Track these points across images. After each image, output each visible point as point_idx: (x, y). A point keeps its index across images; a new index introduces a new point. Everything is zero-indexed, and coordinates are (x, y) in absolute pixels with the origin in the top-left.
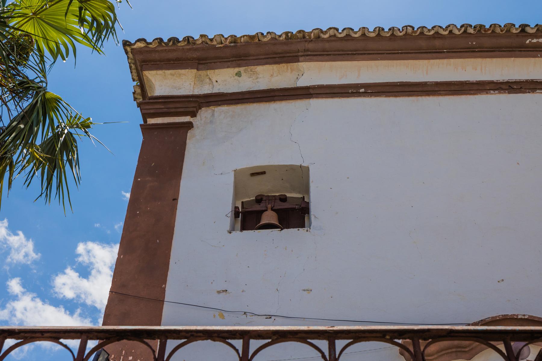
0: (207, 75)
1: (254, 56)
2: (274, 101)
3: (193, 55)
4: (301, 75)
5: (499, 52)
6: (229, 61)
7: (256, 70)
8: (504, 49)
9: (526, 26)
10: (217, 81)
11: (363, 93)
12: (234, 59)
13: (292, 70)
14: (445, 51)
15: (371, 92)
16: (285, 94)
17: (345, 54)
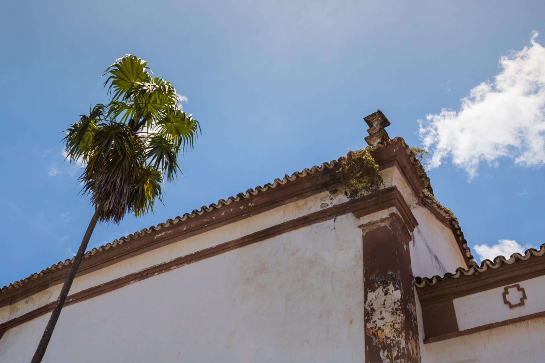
8: (159, 242)
11: (207, 226)
12: (25, 293)
14: (115, 257)
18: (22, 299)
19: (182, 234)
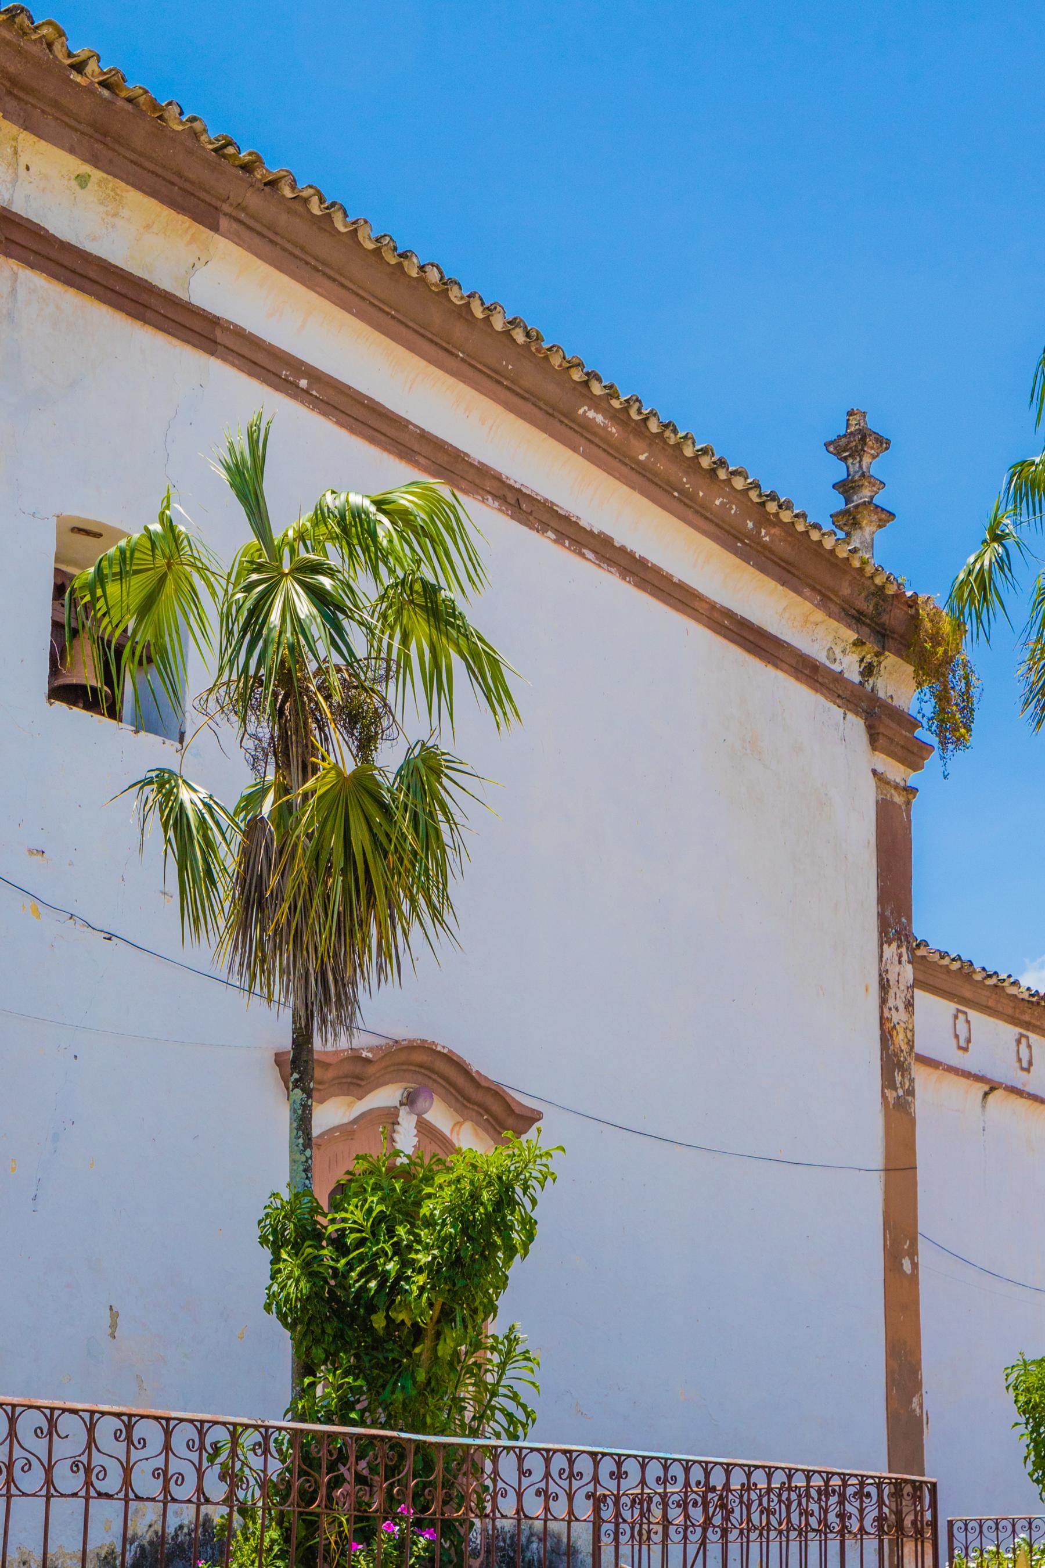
0: (15, 139)
1: (134, 150)
2: (145, 321)
3: (8, 64)
4: (203, 261)
5: (533, 407)
6: (76, 130)
7: (124, 194)
9: (597, 380)
10: (28, 168)
13: (193, 239)
15: (316, 397)
16: (169, 316)
17: (301, 260)
18: (72, 151)
19: (627, 461)
